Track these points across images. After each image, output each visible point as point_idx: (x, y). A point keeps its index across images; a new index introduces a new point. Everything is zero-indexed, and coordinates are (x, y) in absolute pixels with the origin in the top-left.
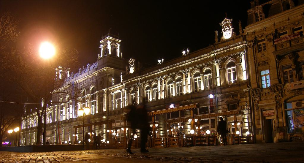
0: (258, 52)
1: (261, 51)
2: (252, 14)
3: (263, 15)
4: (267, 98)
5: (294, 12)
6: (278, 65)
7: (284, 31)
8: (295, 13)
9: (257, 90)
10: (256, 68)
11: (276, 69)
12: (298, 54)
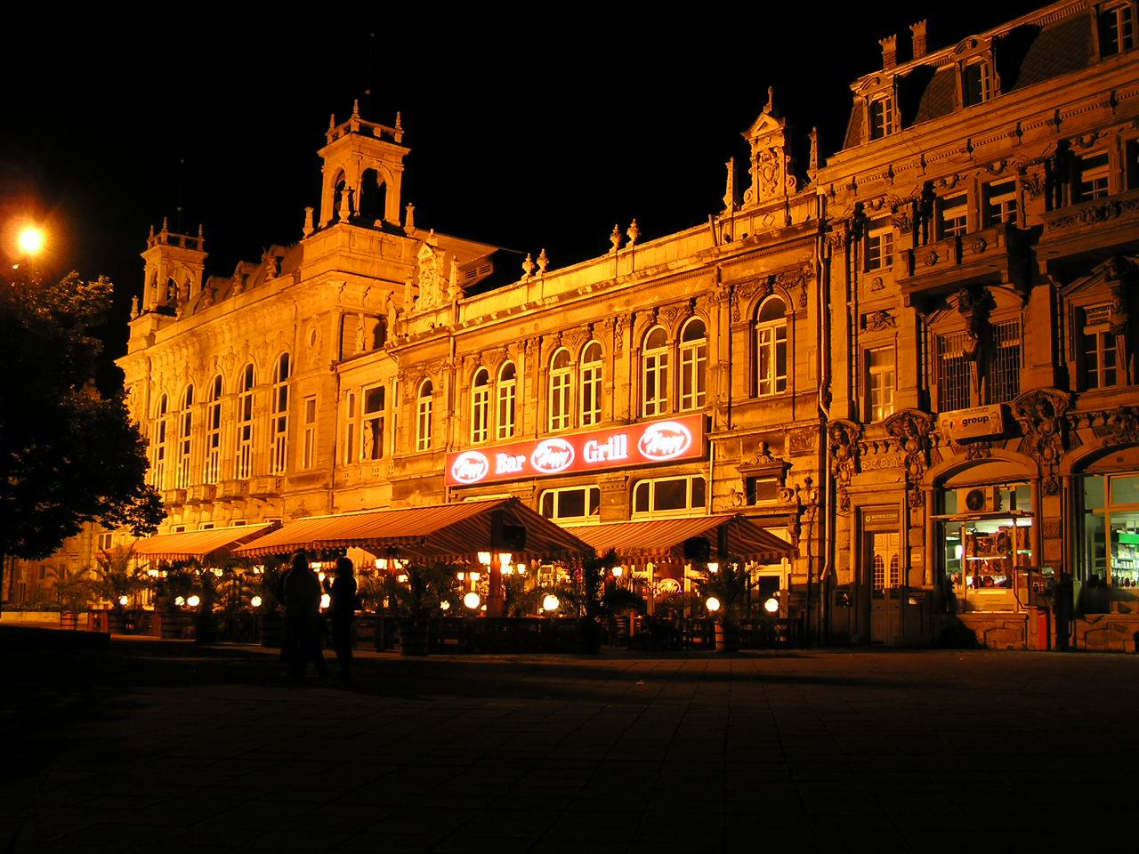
0: (866, 271)
1: (876, 264)
2: (951, 70)
3: (897, 116)
4: (878, 463)
5: (982, 123)
6: (926, 332)
7: (1003, 178)
8: (987, 126)
9: (1052, 397)
10: (850, 336)
11: (914, 350)
12: (990, 293)
